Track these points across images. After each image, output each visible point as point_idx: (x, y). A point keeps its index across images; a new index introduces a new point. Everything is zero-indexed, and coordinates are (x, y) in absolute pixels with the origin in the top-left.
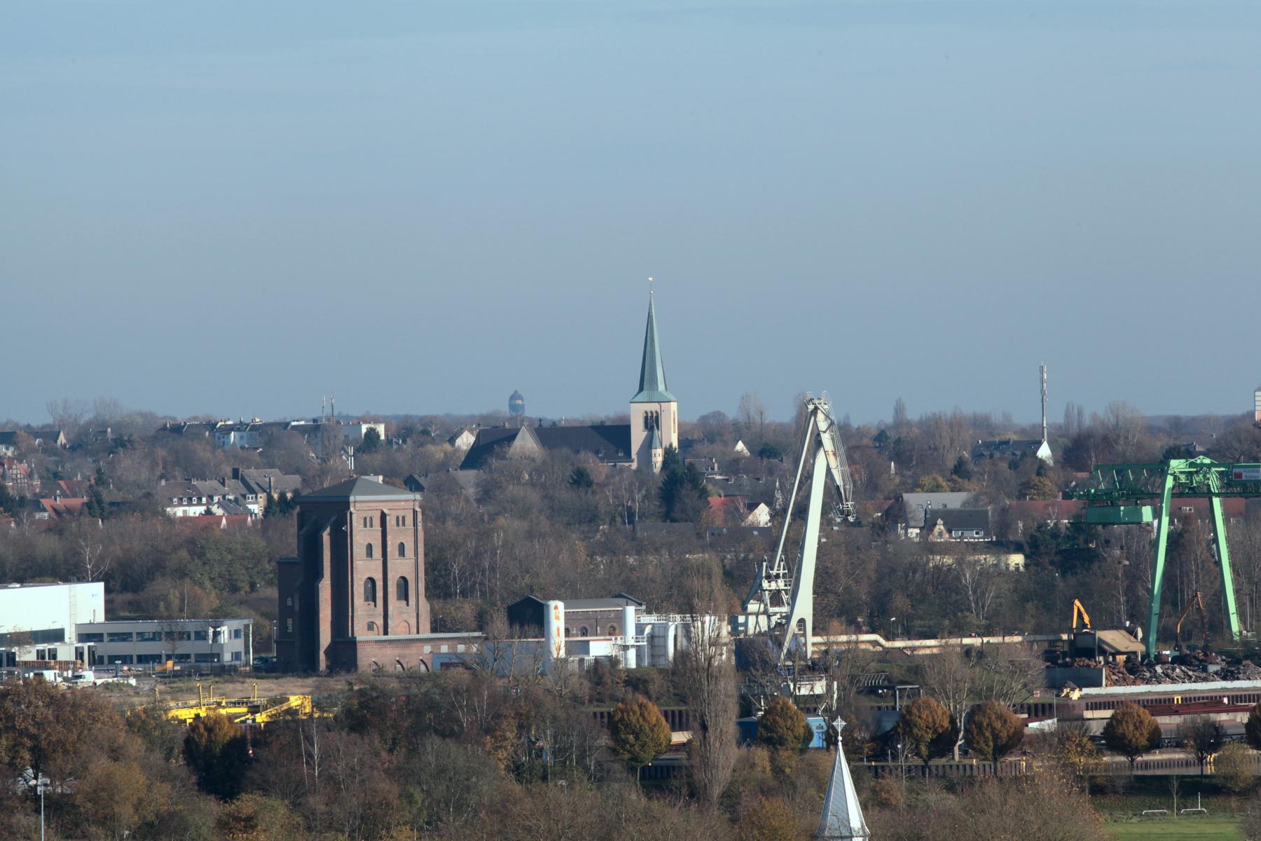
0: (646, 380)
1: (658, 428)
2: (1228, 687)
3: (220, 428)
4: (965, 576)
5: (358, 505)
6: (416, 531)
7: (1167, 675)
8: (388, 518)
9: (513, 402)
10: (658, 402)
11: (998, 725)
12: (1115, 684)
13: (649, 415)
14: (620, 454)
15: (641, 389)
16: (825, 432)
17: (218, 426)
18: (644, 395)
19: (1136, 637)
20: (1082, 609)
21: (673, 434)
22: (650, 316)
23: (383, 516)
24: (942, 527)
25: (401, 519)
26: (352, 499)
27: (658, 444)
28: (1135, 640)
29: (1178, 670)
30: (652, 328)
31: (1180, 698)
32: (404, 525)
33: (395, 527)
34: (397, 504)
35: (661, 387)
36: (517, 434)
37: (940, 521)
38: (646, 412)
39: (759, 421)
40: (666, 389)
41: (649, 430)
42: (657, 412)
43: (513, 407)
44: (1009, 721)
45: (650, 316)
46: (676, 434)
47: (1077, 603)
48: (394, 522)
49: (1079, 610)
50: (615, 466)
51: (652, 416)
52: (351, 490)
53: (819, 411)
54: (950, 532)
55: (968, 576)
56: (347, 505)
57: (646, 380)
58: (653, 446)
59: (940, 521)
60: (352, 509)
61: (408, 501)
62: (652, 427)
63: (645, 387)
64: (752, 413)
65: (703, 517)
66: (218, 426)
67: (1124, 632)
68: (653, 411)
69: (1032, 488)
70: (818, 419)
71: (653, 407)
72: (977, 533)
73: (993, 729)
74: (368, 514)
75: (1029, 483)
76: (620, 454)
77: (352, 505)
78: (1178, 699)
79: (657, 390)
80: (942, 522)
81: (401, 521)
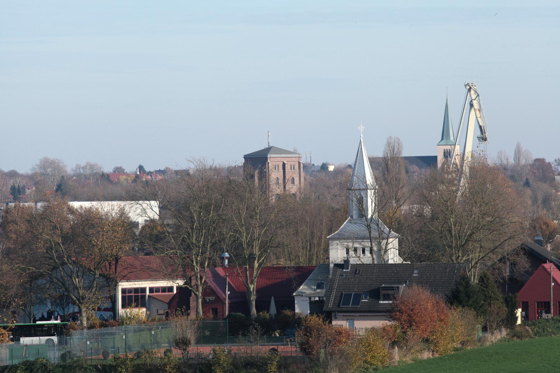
1: (450, 158)
5: (272, 159)
6: (300, 172)
8: (286, 165)
10: (450, 145)
11: (544, 227)
13: (446, 151)
15: (442, 139)
16: (474, 100)
18: (444, 142)
22: (447, 106)
23: (284, 165)
25: (292, 166)
26: (269, 156)
32: (294, 169)
33: (290, 170)
34: (291, 159)
38: (445, 150)
39: (506, 163)
41: (446, 158)
42: (449, 150)
44: (550, 225)
45: (447, 106)
48: (289, 168)
51: (447, 152)
52: (269, 152)
53: (472, 90)
56: (266, 159)
57: (445, 134)
60: (269, 161)
61: (296, 157)
62: (447, 157)
63: (444, 138)
64: (503, 160)
68: (448, 149)
70: (471, 93)
71: (448, 147)
73: (542, 229)
74: (277, 163)
77: (269, 159)
79: (450, 139)
81: (293, 167)
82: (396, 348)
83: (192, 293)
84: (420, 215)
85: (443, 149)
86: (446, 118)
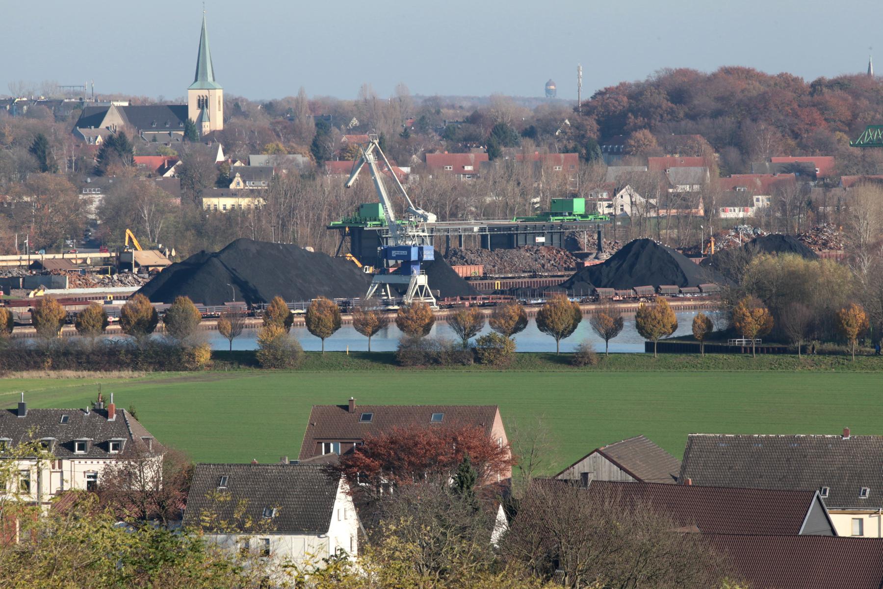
0: (199, 74)
2: (85, 292)
3: (16, 103)
4: (144, 212)
7: (121, 281)
9: (548, 87)
12: (77, 287)
13: (201, 98)
14: (181, 126)
15: (196, 80)
17: (16, 101)
19: (165, 254)
20: (132, 236)
21: (218, 112)
22: (203, 29)
24: (239, 179)
27: (207, 119)
28: (164, 257)
29: (130, 278)
30: (204, 37)
31: (499, 282)
35: (210, 79)
36: (107, 111)
37: (238, 174)
38: (199, 96)
40: (214, 80)
42: (206, 96)
43: (548, 91)
45: (203, 29)
46: (221, 112)
47: (128, 231)
49: (130, 238)
50: (170, 134)
51: (203, 99)
54: (244, 182)
55: (146, 212)
57: (199, 74)
58: (203, 120)
59: (238, 174)
65: (108, 170)
66: (16, 101)
67: (157, 252)
68: (204, 95)
69: (348, 152)
71: (204, 93)
72: (264, 183)
75: (346, 149)
76: (181, 126)
78: (498, 283)
79: (207, 81)
80: (239, 175)
82: (342, 140)
83: (37, 295)
84: (540, 310)
85: (197, 95)
86: (202, 45)
